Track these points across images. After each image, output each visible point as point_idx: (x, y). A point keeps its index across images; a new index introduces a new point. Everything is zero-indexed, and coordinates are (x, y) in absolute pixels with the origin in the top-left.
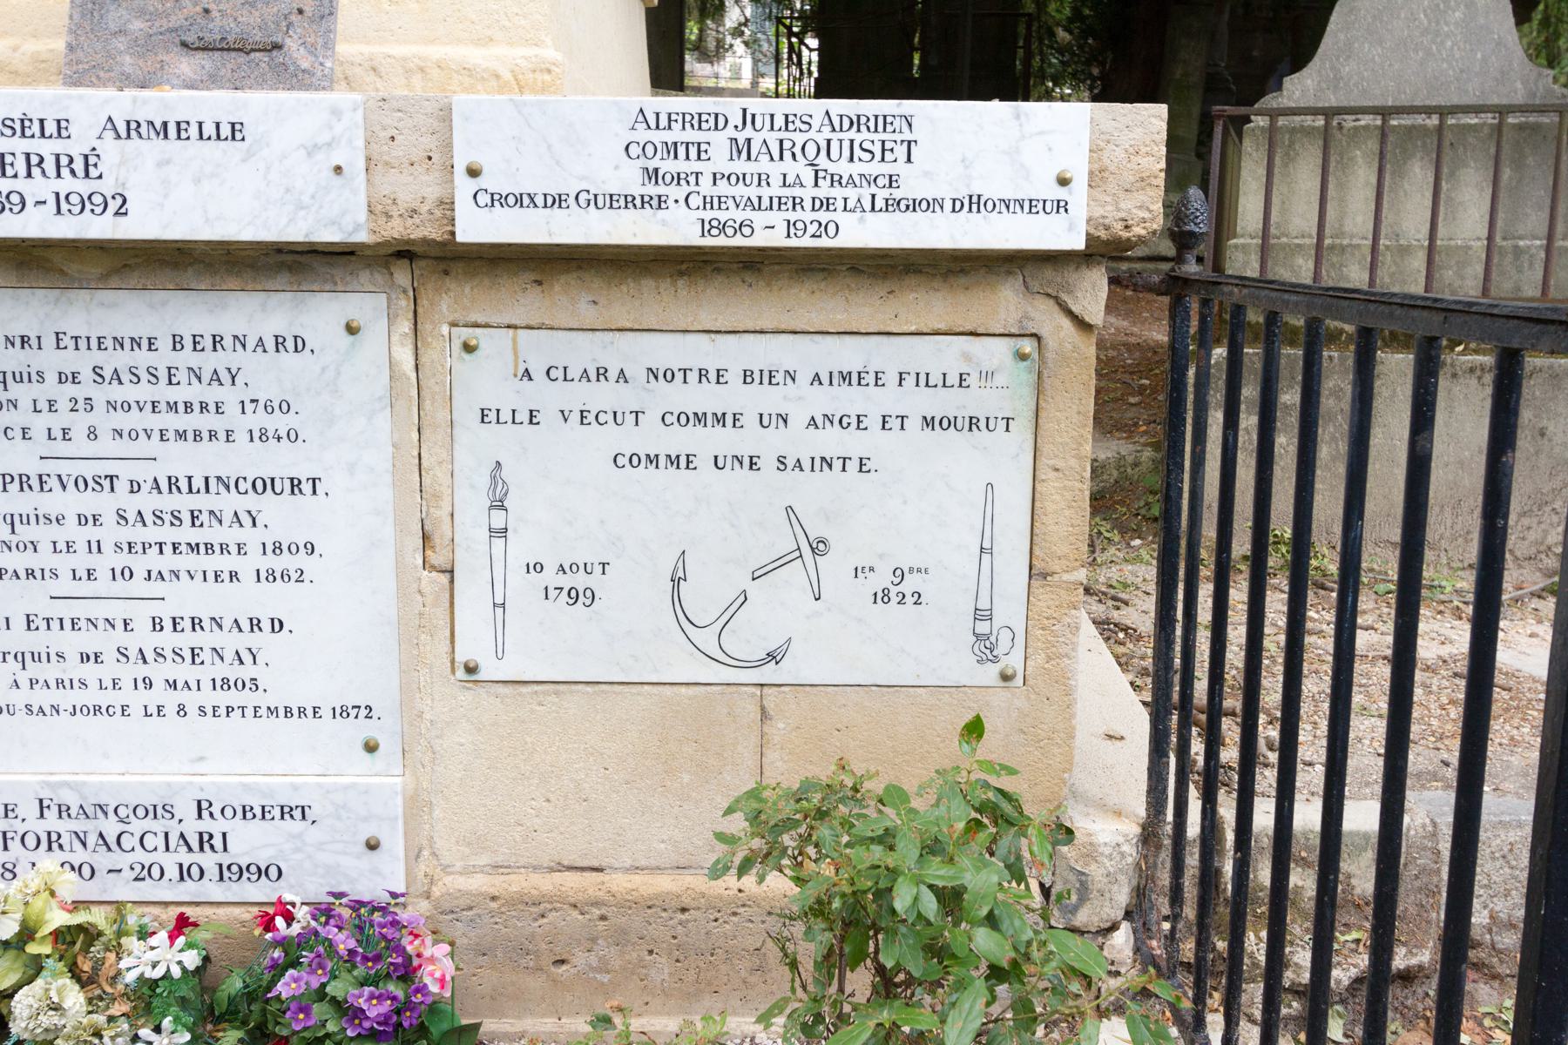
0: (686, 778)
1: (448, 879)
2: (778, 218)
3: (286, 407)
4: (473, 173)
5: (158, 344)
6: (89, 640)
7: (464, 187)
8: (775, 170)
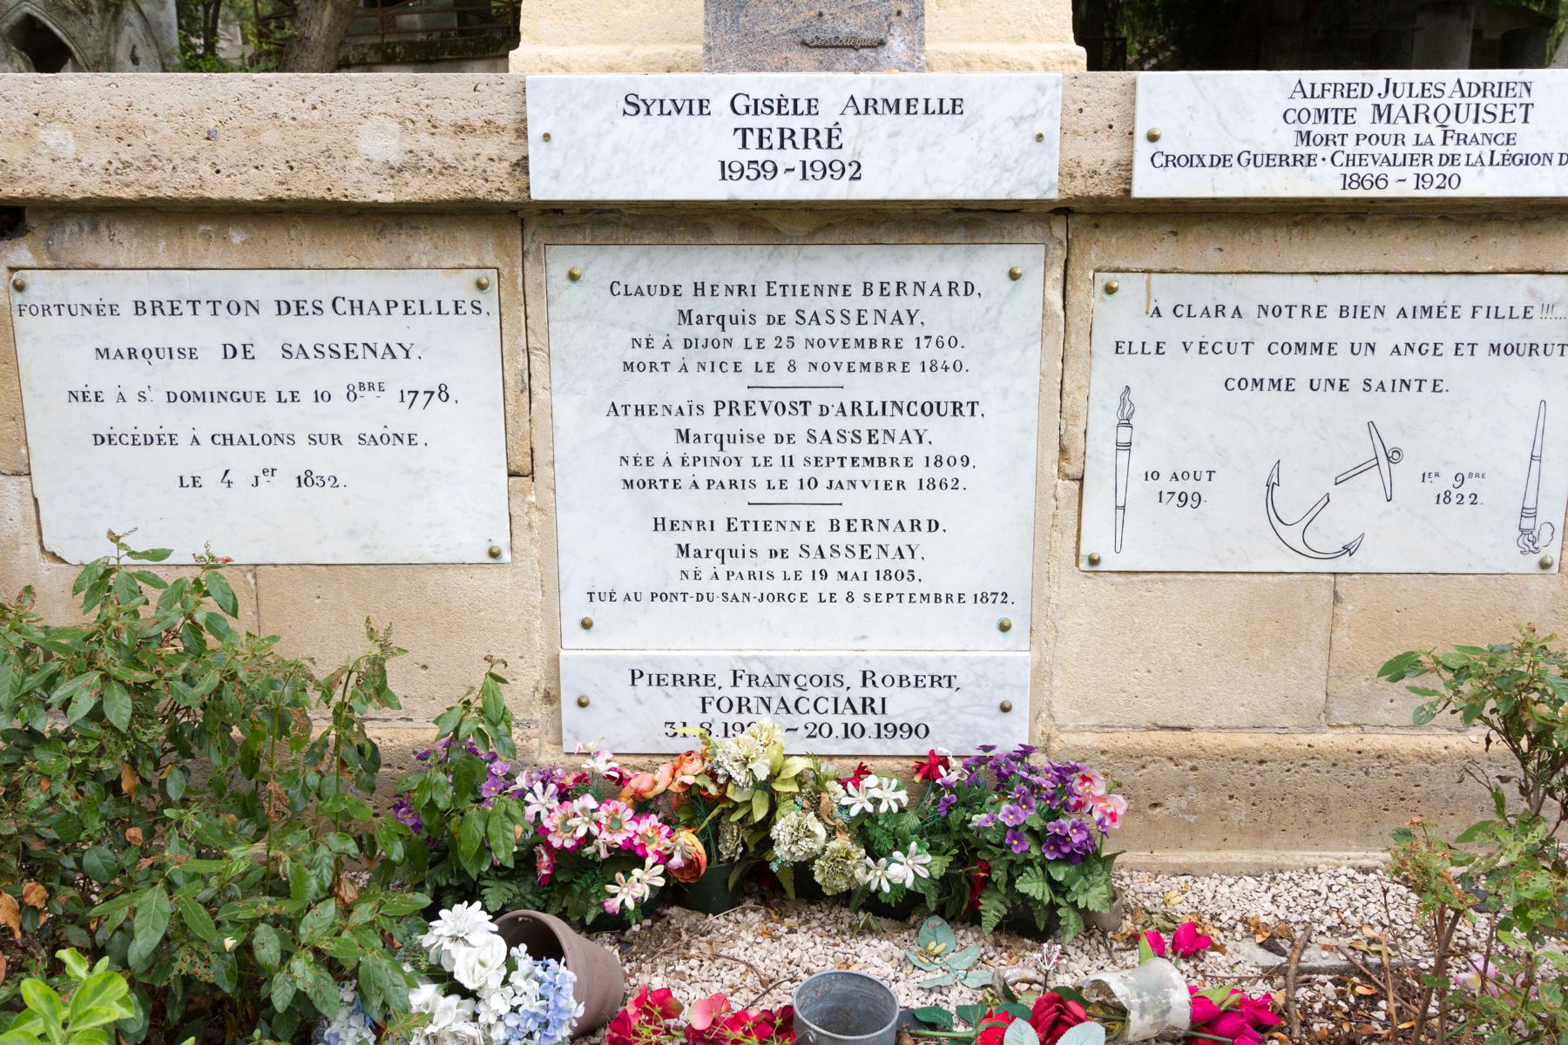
0: (1267, 652)
1: (1063, 737)
2: (1409, 173)
3: (953, 342)
4: (1153, 138)
5: (851, 290)
6: (777, 539)
7: (1143, 149)
8: (1409, 131)
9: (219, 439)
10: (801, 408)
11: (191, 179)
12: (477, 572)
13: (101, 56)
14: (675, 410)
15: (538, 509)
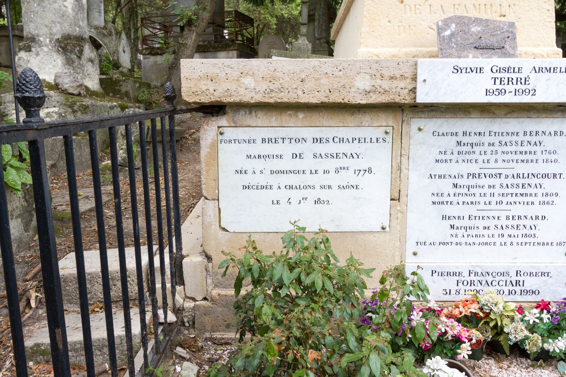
3: (555, 152)
5: (519, 134)
6: (486, 223)
9: (288, 187)
10: (498, 176)
11: (294, 96)
12: (376, 235)
13: (116, 50)
14: (453, 176)
15: (400, 212)
